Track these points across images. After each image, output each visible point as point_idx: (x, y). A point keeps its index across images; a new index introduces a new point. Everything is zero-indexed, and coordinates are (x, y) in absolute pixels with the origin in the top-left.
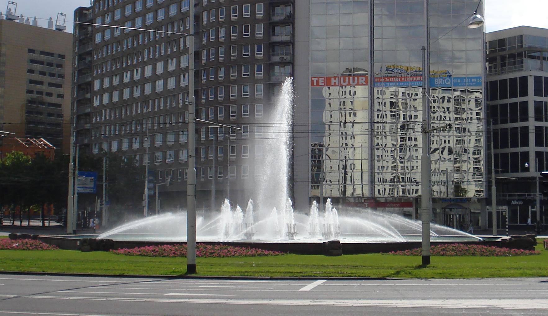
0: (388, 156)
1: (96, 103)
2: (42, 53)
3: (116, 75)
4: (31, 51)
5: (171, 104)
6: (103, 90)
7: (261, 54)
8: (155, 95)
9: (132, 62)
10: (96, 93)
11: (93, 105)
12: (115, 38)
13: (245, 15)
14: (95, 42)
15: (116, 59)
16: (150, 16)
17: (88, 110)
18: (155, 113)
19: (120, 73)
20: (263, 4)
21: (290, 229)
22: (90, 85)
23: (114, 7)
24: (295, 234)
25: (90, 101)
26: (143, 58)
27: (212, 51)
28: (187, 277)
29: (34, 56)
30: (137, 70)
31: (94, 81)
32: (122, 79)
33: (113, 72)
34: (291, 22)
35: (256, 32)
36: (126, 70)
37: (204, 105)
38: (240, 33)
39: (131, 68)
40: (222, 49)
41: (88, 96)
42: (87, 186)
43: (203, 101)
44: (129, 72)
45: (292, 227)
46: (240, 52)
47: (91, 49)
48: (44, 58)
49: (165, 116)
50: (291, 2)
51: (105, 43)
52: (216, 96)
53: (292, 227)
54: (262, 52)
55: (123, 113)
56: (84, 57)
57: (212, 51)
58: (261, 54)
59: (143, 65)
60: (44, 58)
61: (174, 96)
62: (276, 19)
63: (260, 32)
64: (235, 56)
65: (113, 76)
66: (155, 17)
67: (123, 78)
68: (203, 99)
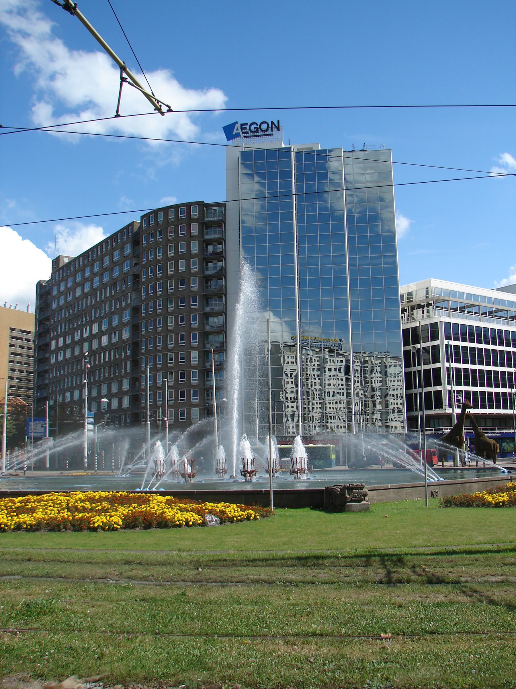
0: (330, 403)
1: (53, 361)
2: (21, 331)
3: (69, 335)
4: (12, 329)
5: (115, 356)
6: (58, 349)
7: (197, 399)
8: (101, 349)
9: (82, 321)
10: (52, 352)
11: (50, 362)
12: (68, 303)
13: (181, 270)
14: (52, 308)
15: (70, 320)
16: (97, 280)
17: (47, 368)
18: (101, 365)
19: (71, 332)
20: (197, 259)
21: (246, 466)
22: (48, 345)
23: (67, 276)
24: (254, 473)
25: (48, 359)
26: (91, 317)
27: (151, 304)
28: (330, 471)
29: (16, 334)
30: (86, 329)
31: (51, 342)
32: (73, 337)
33: (66, 332)
34: (223, 275)
35: (191, 249)
36: (76, 329)
37: (143, 354)
38: (177, 286)
39: (81, 328)
40: (160, 301)
41: (47, 355)
42: (38, 431)
43: (143, 351)
44: (79, 331)
45: (249, 464)
46: (177, 286)
47: (49, 315)
48: (21, 335)
49: (109, 368)
50: (223, 275)
51: (60, 308)
52: (155, 346)
53: (249, 464)
54: (198, 398)
55: (75, 367)
56: (43, 322)
57: (151, 304)
58: (197, 399)
59: (90, 323)
60: (21, 335)
61: (117, 348)
62: (208, 328)
63: (195, 286)
64: (172, 307)
65: (66, 336)
66: (101, 279)
67: (74, 337)
68: (143, 349)
